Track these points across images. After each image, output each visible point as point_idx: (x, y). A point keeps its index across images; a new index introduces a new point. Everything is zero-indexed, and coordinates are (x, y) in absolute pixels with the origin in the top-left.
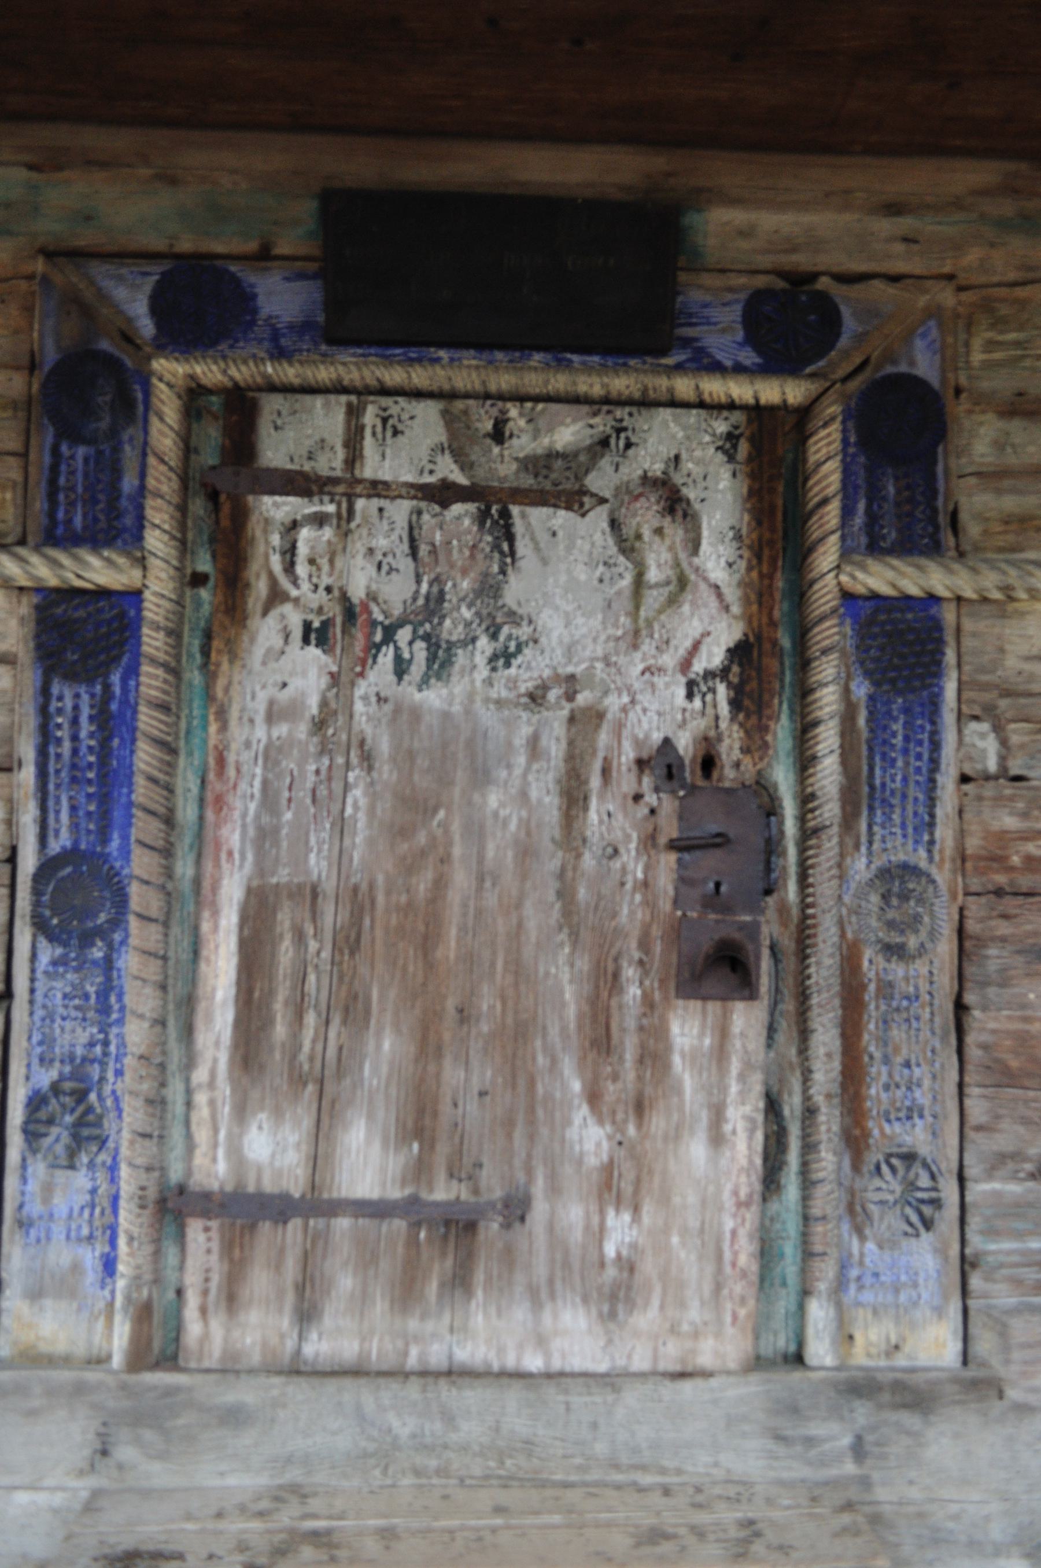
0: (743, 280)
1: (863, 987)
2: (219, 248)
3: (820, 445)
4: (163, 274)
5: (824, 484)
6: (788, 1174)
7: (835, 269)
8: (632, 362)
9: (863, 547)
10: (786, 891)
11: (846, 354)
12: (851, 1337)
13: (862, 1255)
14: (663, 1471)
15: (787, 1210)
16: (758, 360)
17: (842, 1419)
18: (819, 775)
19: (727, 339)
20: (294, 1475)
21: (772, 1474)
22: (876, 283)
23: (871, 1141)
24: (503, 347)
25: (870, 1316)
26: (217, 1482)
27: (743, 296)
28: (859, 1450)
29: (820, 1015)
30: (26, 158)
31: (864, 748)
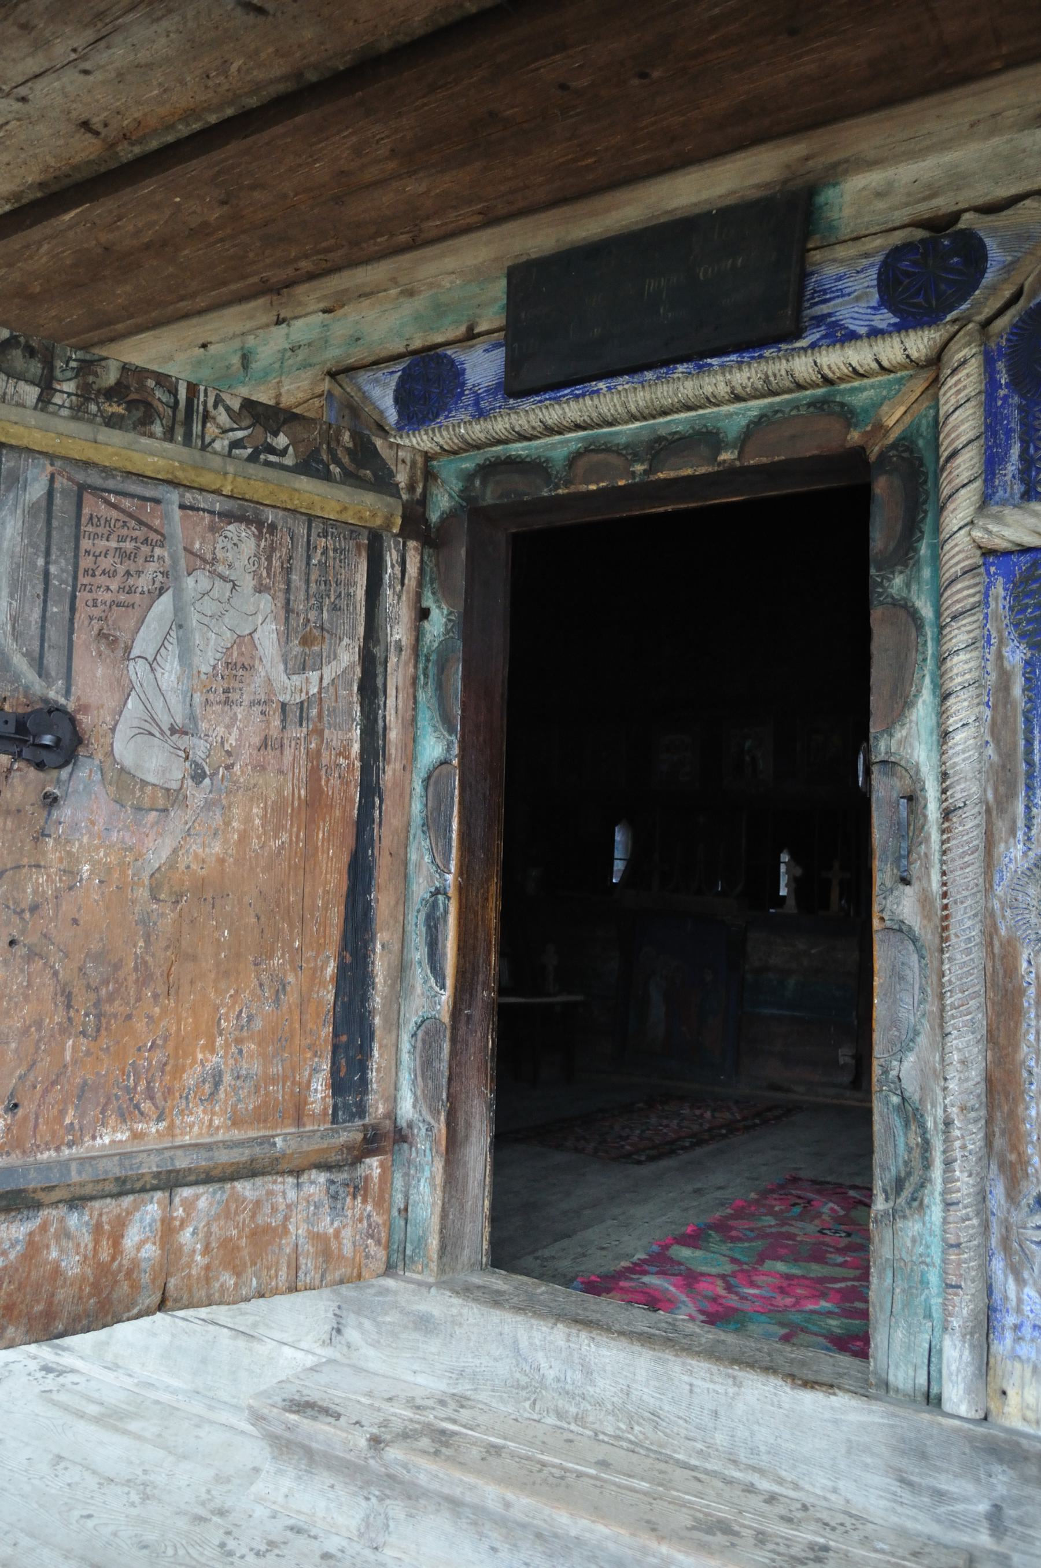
0: (878, 242)
1: (1021, 992)
2: (440, 339)
3: (949, 394)
4: (404, 370)
5: (953, 436)
6: (932, 1193)
7: (980, 201)
8: (767, 353)
9: (1017, 496)
10: (929, 881)
11: (994, 289)
12: (1004, 1393)
13: (1020, 1301)
14: (780, 1481)
15: (931, 1233)
16: (897, 320)
17: (978, 1480)
18: (951, 752)
19: (861, 307)
20: (464, 1387)
21: (895, 1519)
22: (1027, 202)
23: (1031, 1170)
24: (649, 367)
25: (1028, 1374)
26: (410, 1377)
27: (879, 258)
28: (995, 1519)
29: (953, 1017)
30: (322, 305)
31: (1021, 719)
